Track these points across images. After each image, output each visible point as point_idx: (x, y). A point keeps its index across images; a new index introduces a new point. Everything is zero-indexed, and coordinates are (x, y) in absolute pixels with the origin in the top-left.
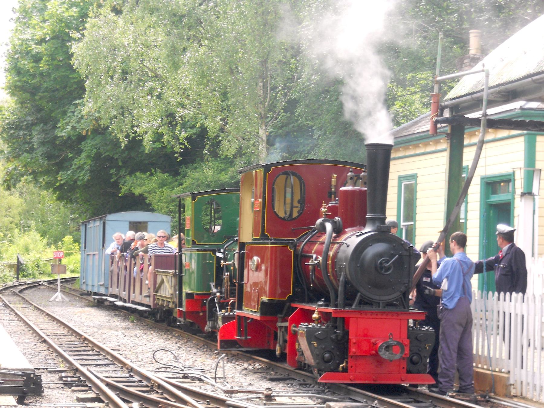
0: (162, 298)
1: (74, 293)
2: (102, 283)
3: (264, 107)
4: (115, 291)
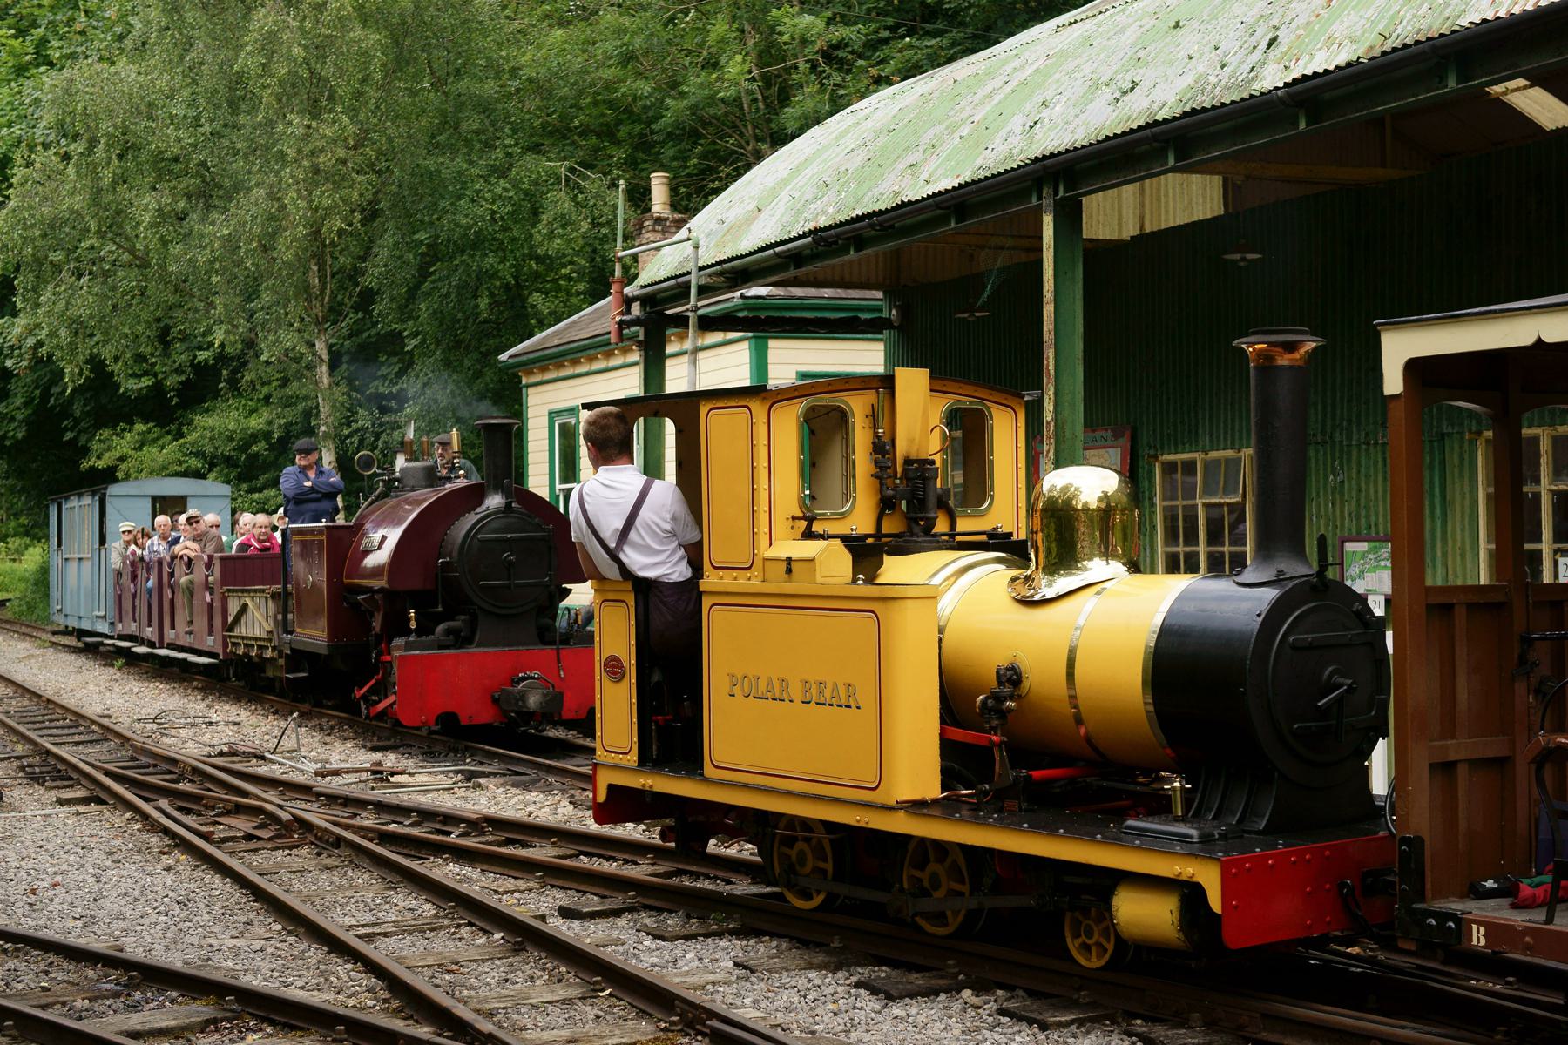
0: (259, 643)
1: (8, 627)
2: (102, 613)
3: (322, 305)
4: (133, 628)
